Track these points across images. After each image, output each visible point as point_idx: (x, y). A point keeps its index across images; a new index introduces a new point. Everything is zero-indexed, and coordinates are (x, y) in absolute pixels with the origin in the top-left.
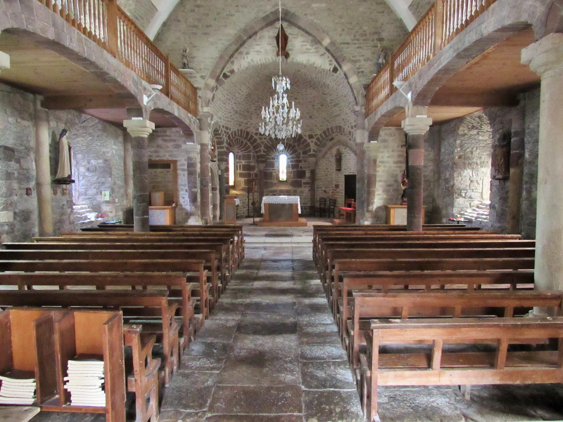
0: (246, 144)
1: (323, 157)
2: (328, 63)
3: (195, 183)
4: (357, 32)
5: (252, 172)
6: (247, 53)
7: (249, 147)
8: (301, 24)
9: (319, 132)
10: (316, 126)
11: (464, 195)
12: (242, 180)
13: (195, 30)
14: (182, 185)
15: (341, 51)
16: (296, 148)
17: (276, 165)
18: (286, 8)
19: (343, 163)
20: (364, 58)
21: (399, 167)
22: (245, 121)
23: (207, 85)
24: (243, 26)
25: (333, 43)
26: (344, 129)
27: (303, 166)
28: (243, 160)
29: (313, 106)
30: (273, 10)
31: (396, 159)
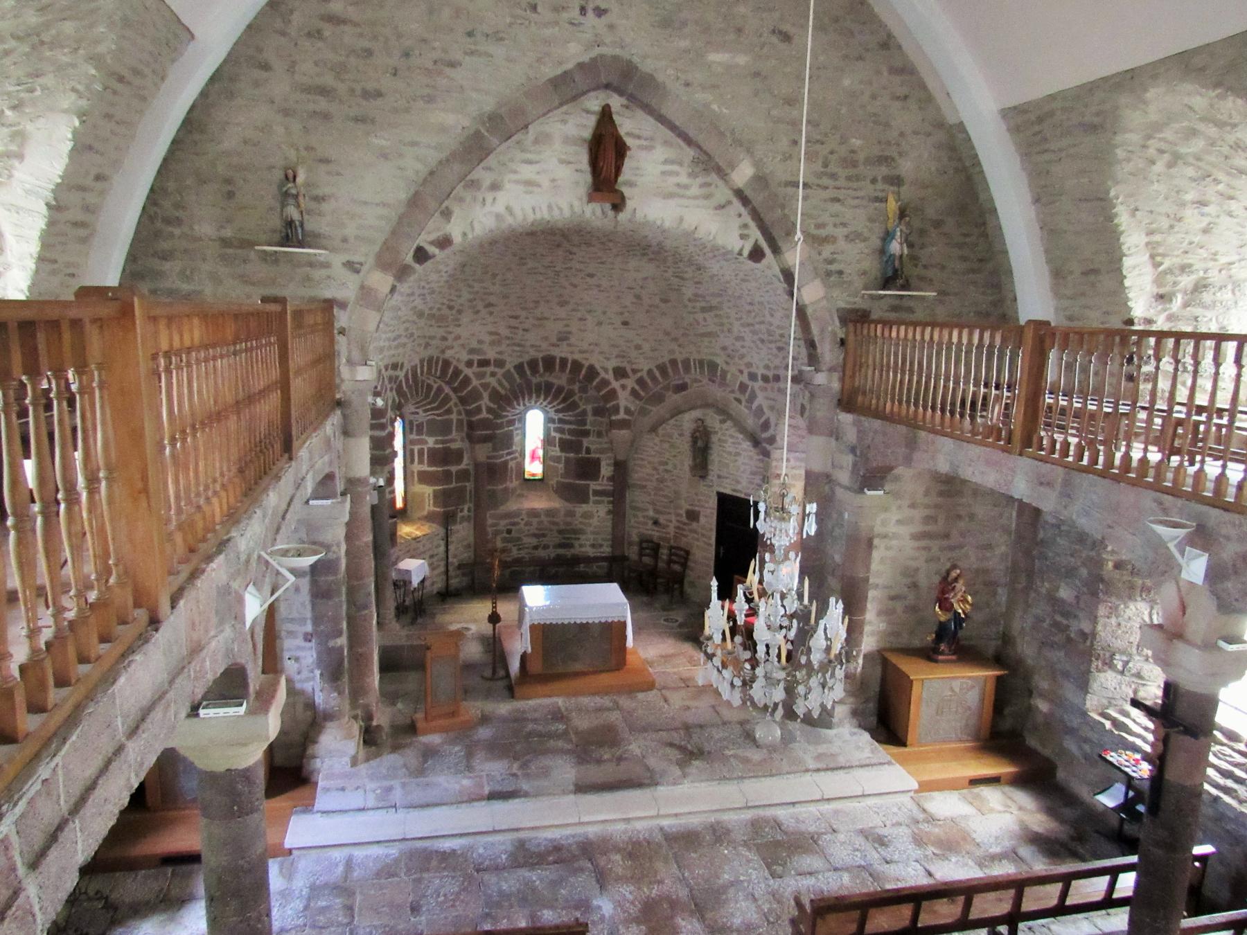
0: (440, 390)
1: (653, 429)
2: (736, 233)
3: (336, 620)
4: (832, 153)
5: (454, 469)
6: (495, 187)
7: (447, 399)
8: (669, 110)
9: (645, 366)
10: (638, 347)
11: (1120, 667)
12: (428, 490)
13: (322, 104)
14: (292, 620)
15: (783, 207)
16: (576, 398)
17: (517, 439)
18: (626, 56)
19: (714, 457)
20: (845, 231)
21: (924, 548)
22: (441, 332)
23: (366, 292)
24: (489, 105)
25: (761, 180)
26: (724, 373)
27: (593, 447)
28: (430, 434)
29: (638, 297)
30: (586, 58)
31: (917, 528)
